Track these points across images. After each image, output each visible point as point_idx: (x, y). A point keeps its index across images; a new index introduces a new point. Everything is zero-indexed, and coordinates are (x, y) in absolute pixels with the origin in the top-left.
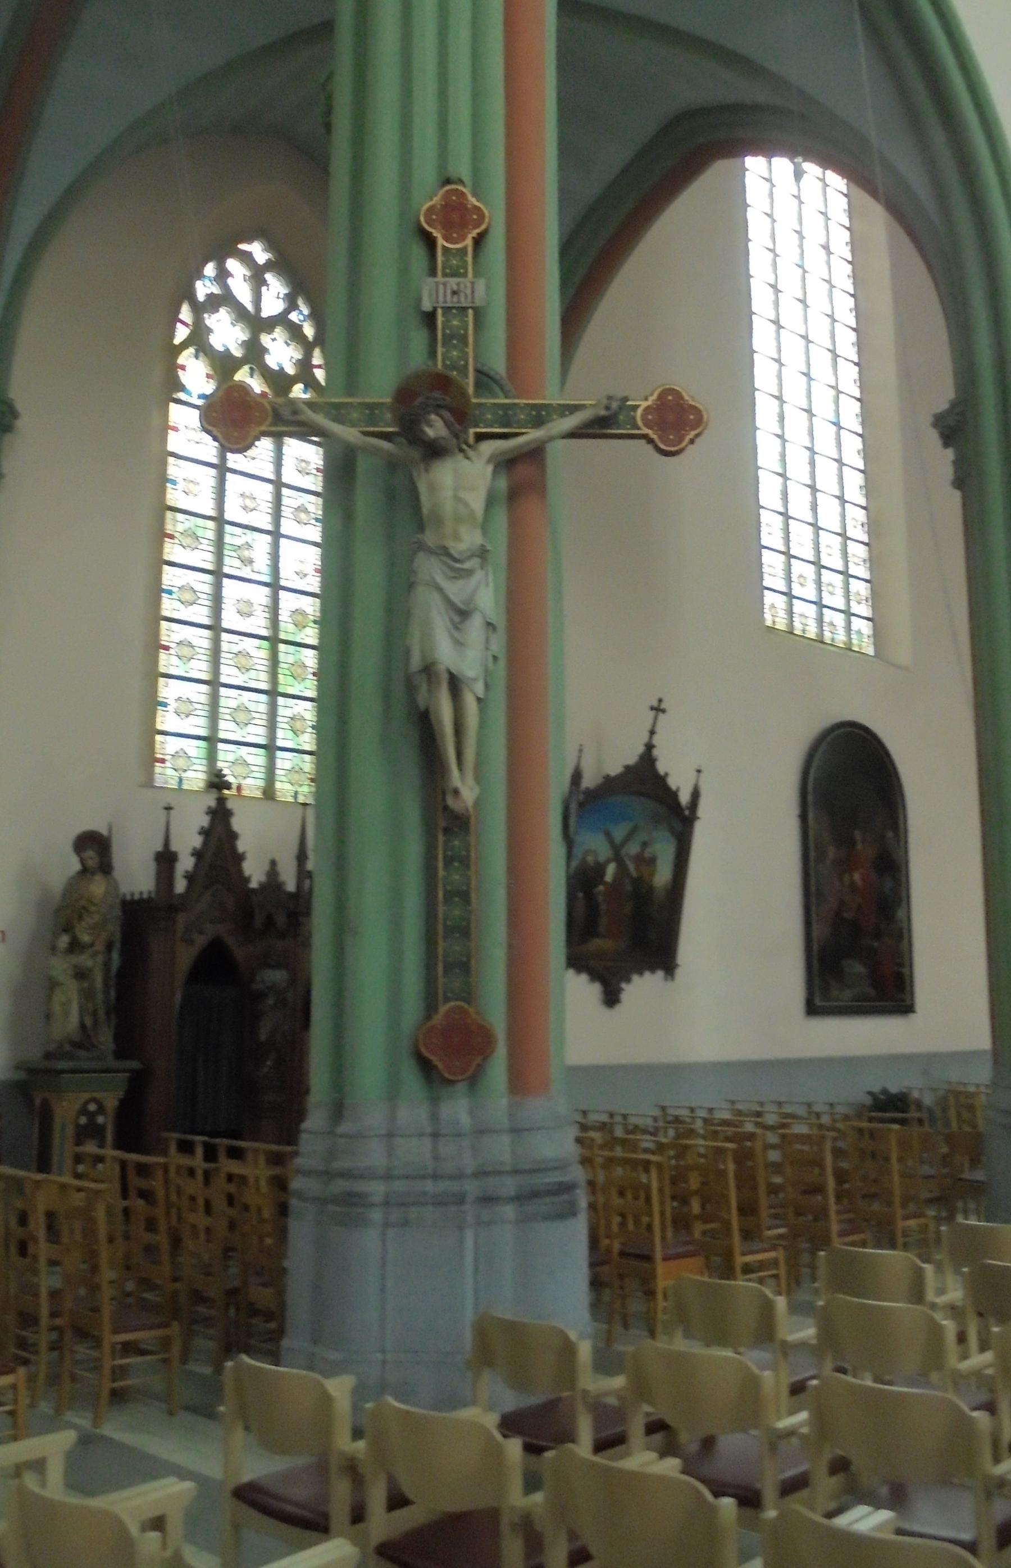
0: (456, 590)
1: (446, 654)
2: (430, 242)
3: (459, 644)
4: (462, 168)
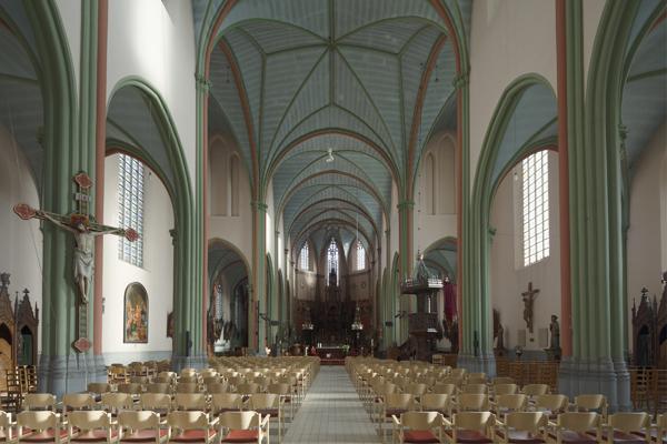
0: (86, 260)
1: (84, 273)
2: (78, 185)
3: (87, 271)
4: (85, 169)
